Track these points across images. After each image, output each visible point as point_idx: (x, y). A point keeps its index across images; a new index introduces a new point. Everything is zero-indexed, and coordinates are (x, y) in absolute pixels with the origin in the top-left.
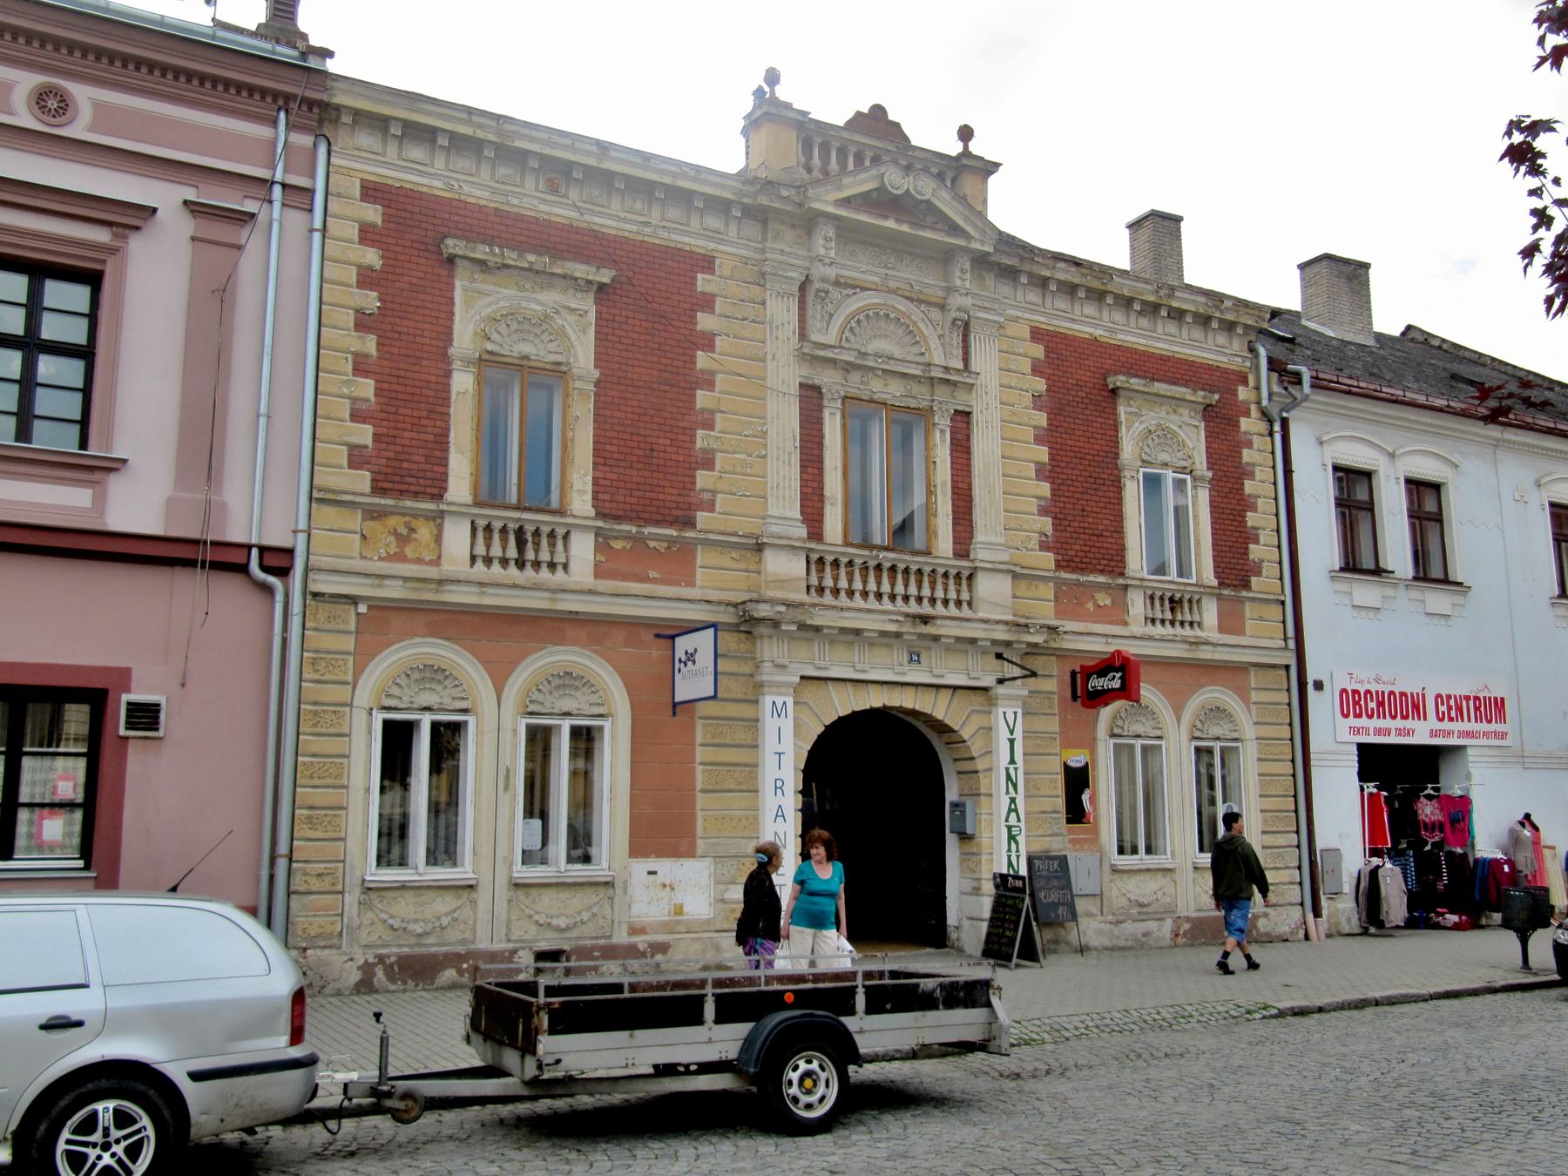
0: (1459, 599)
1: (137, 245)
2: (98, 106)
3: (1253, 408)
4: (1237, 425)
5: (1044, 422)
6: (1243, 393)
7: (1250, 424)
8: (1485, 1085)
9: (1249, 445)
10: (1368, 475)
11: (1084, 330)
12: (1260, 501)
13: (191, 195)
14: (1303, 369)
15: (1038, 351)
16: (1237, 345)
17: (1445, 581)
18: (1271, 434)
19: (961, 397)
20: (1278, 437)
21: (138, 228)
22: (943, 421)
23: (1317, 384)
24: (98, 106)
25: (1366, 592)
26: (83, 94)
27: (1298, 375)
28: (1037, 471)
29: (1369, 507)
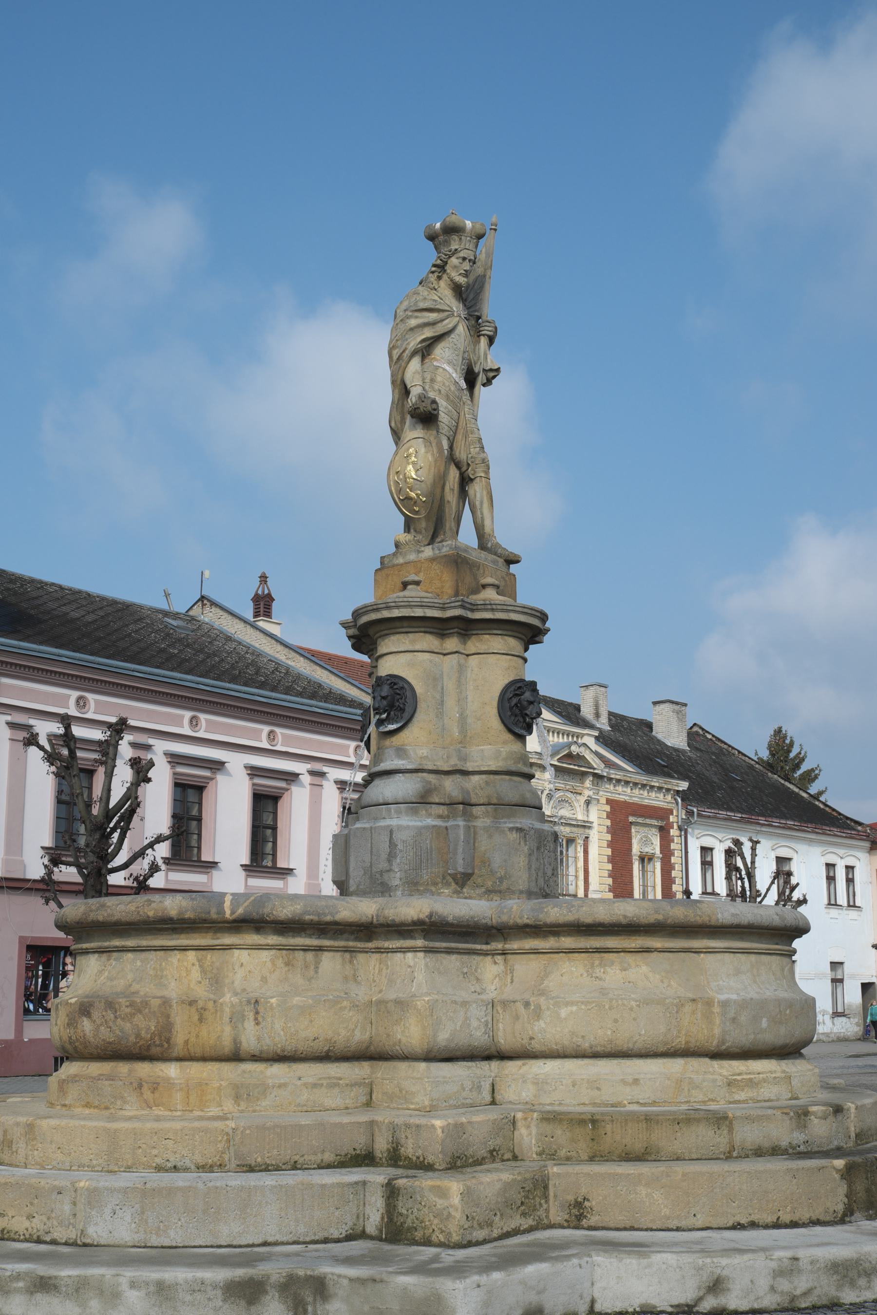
0: (859, 913)
1: (295, 789)
2: (96, 701)
3: (675, 825)
4: (669, 833)
5: (610, 839)
6: (672, 819)
7: (674, 832)
8: (759, 1300)
9: (673, 841)
10: (711, 849)
11: (622, 798)
12: (676, 865)
13: (9, 718)
14: (695, 810)
15: (608, 808)
16: (669, 798)
17: (836, 905)
18: (681, 836)
19: (587, 831)
20: (683, 837)
21: (293, 781)
22: (580, 841)
23: (699, 815)
24: (206, 720)
25: (834, 912)
26: (91, 697)
27: (693, 812)
28: (608, 859)
29: (711, 864)
